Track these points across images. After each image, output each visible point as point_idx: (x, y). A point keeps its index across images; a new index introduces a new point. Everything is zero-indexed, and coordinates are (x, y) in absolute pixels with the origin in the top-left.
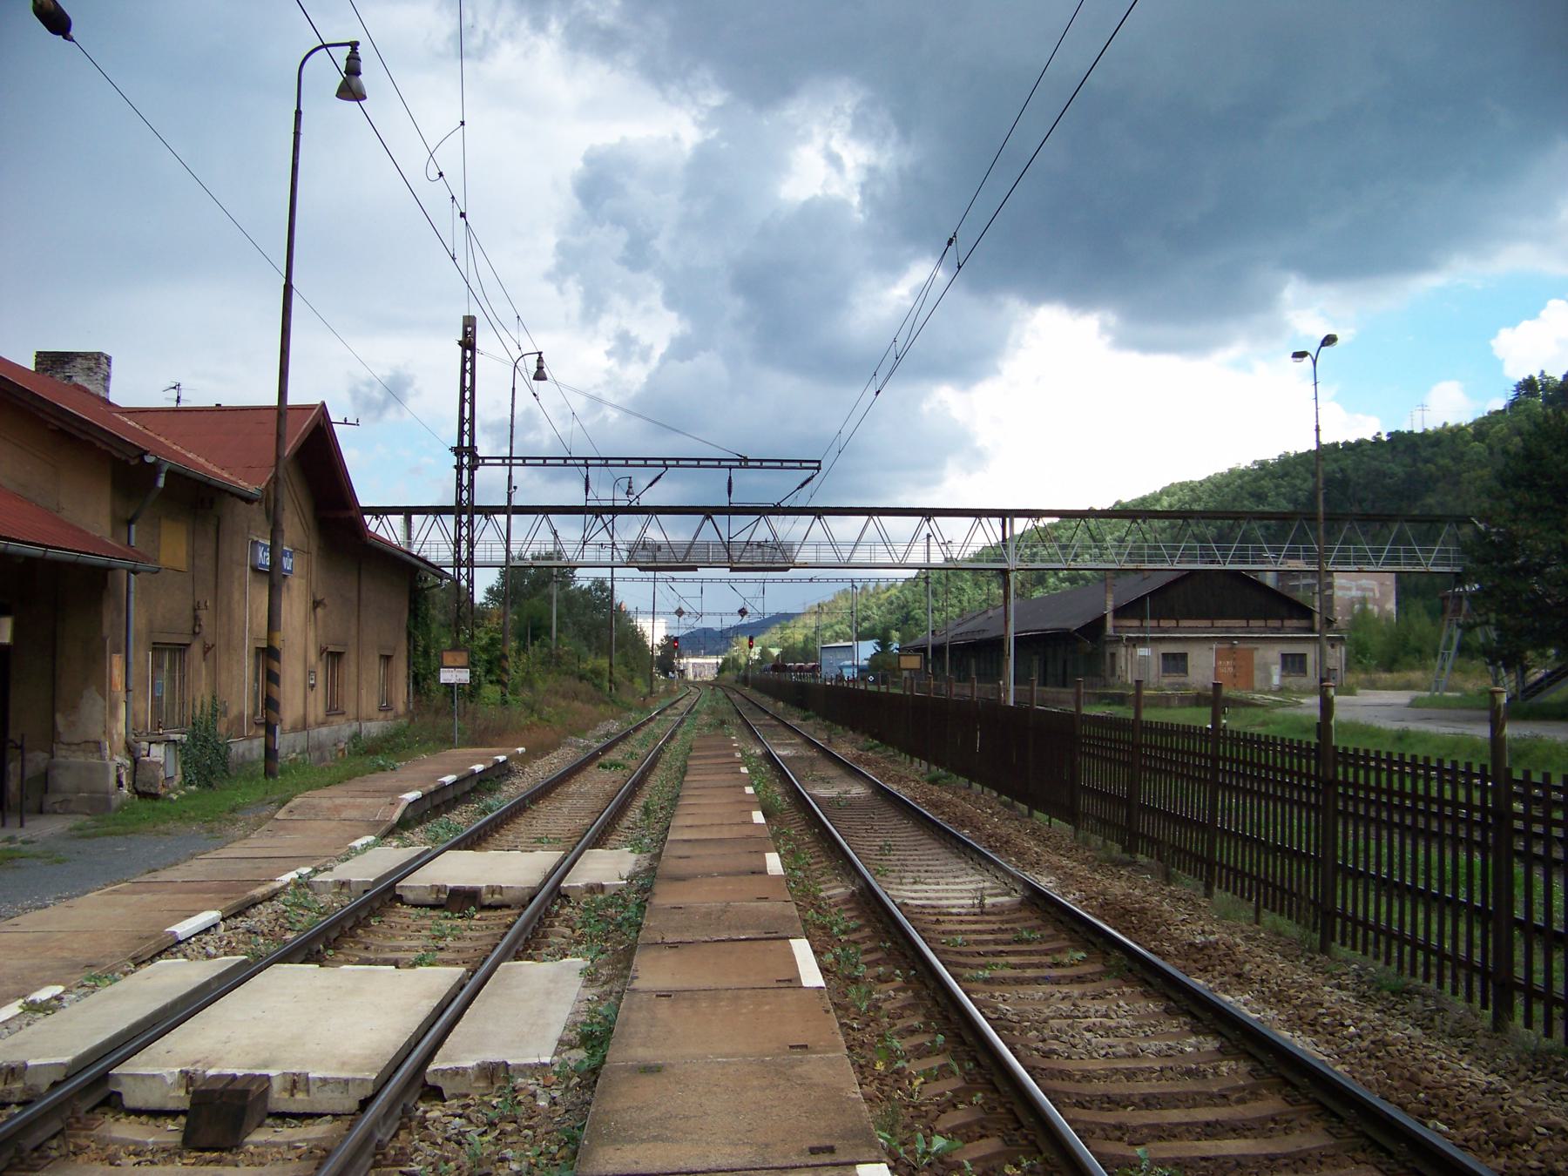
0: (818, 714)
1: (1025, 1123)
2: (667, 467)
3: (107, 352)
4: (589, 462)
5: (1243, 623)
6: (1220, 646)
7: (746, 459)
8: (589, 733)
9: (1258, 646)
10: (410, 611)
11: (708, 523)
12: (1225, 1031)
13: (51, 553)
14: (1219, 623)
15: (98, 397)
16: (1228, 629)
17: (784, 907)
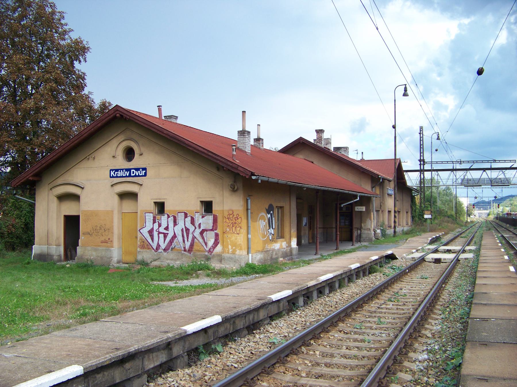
2: (474, 163)
3: (348, 147)
4: (454, 162)
7: (495, 161)
8: (454, 231)
10: (411, 201)
11: (484, 173)
13: (366, 195)
15: (347, 156)
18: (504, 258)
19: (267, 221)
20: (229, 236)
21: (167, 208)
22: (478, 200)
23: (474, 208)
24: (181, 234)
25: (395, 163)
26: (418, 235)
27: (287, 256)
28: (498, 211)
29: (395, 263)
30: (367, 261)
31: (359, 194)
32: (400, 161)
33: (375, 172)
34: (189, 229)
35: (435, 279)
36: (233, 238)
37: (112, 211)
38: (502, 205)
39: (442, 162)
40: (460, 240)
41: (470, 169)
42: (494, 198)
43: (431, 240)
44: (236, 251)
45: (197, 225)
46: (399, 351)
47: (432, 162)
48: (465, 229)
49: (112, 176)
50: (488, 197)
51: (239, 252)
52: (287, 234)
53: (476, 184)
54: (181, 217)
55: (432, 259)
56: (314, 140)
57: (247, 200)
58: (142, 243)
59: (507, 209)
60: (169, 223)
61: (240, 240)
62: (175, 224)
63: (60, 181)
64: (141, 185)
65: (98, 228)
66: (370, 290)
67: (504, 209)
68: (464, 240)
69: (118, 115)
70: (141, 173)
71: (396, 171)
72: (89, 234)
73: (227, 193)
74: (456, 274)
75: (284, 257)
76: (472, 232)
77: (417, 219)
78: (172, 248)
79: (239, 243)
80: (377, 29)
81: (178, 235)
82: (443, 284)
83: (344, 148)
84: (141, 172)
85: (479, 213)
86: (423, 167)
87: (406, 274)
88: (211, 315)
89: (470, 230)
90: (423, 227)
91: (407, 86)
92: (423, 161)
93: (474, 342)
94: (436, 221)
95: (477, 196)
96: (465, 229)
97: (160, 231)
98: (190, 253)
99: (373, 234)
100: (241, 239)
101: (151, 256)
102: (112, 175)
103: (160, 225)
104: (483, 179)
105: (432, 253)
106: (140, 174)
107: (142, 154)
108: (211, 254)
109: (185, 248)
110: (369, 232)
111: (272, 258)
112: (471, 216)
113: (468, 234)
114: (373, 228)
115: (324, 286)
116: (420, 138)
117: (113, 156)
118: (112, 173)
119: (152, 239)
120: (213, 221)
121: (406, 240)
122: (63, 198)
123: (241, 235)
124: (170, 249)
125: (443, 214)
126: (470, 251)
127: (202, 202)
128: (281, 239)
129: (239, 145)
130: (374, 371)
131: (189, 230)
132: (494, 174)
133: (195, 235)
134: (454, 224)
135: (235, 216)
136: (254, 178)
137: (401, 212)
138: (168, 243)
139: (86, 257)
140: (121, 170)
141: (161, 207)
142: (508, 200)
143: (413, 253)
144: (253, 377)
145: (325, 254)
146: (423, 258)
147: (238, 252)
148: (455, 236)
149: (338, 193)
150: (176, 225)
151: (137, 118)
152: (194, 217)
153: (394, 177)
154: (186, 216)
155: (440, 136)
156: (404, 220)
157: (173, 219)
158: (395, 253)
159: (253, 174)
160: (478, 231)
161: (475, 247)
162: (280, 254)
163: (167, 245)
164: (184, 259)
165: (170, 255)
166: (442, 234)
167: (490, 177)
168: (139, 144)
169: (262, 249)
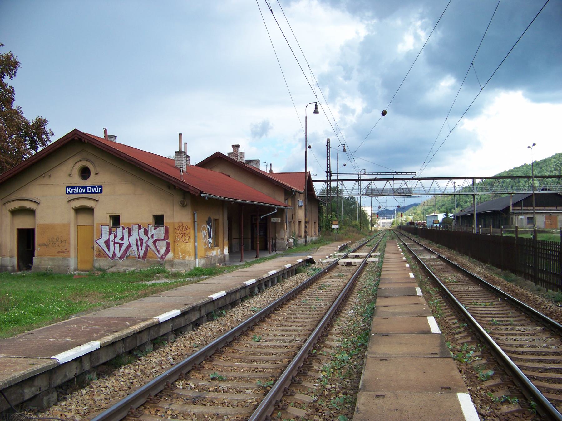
0: (420, 236)
1: (493, 355)
5: (555, 208)
6: (546, 215)
7: (398, 173)
9: (559, 215)
11: (388, 183)
12: (545, 324)
14: (547, 208)
16: (550, 210)
17: (425, 306)
18: (402, 259)
19: (207, 231)
20: (179, 244)
21: (122, 221)
22: (382, 209)
23: (377, 217)
24: (135, 244)
25: (306, 176)
26: (328, 244)
27: (222, 262)
28: (402, 220)
29: (313, 266)
30: (265, 276)
31: (277, 207)
32: (310, 174)
33: (289, 185)
34: (143, 240)
35: (349, 277)
36: (183, 246)
37: (69, 225)
38: (405, 214)
39: (348, 174)
40: (365, 248)
41: (375, 179)
42: (397, 208)
43: (340, 248)
44: (186, 257)
45: (150, 235)
46: (283, 392)
47: (338, 173)
48: (369, 238)
49: (68, 192)
50: (392, 206)
51: (189, 258)
52: (221, 243)
53: (381, 193)
54: (135, 229)
55: (344, 262)
56: (228, 154)
57: (194, 214)
58: (99, 253)
59: (410, 218)
60: (124, 235)
61: (189, 248)
62: (130, 234)
63: (14, 197)
64: (97, 201)
65: (55, 240)
66: (302, 284)
67: (406, 218)
68: (369, 248)
69: (76, 138)
70: (97, 190)
71: (307, 184)
72: (45, 245)
73: (177, 208)
74: (365, 273)
75: (219, 263)
76: (376, 241)
77: (324, 229)
78: (127, 256)
79: (188, 250)
80: (316, 97)
81: (133, 244)
82: (357, 278)
83: (255, 160)
84: (97, 189)
85: (383, 223)
86: (330, 178)
87: (326, 273)
88: (220, 291)
89: (374, 239)
90: (330, 237)
91: (318, 104)
92: (330, 172)
93: (381, 297)
94: (342, 231)
95: (381, 205)
96: (369, 238)
97: (115, 241)
98: (144, 260)
99: (286, 243)
100: (189, 247)
101: (107, 263)
102: (69, 192)
103: (115, 236)
104: (386, 189)
105: (351, 253)
106: (96, 191)
107: (98, 173)
108: (163, 260)
109: (139, 255)
110: (283, 242)
111: (211, 264)
112: (375, 226)
113: (374, 243)
114: (286, 238)
115: (268, 280)
116: (327, 150)
117: (69, 175)
118: (68, 190)
119: (109, 249)
120: (165, 232)
121: (318, 248)
122: (15, 212)
123: (190, 243)
124: (126, 256)
125: (348, 224)
126: (375, 256)
127: (154, 215)
128: (217, 248)
129: (177, 164)
130: (279, 382)
131: (142, 240)
132: (397, 185)
133: (148, 244)
134: (359, 234)
135: (185, 228)
136: (202, 195)
137: (310, 223)
138: (123, 252)
139: (43, 267)
140: (77, 187)
141: (116, 221)
142: (411, 209)
143: (327, 259)
144: (200, 362)
145: (249, 261)
146: (337, 262)
147: (187, 258)
148: (361, 245)
149: (257, 206)
150: (131, 236)
151: (94, 141)
152: (148, 229)
153: (305, 190)
154: (140, 228)
155: (346, 147)
156: (312, 230)
157: (128, 230)
158: (314, 258)
159: (202, 193)
160: (382, 240)
161: (380, 253)
162: (217, 260)
163: (122, 254)
164: (139, 265)
165: (126, 262)
166: (349, 243)
167: (393, 187)
168: (95, 165)
169: (204, 255)
